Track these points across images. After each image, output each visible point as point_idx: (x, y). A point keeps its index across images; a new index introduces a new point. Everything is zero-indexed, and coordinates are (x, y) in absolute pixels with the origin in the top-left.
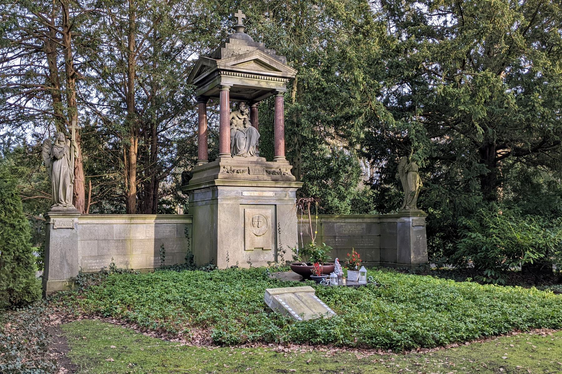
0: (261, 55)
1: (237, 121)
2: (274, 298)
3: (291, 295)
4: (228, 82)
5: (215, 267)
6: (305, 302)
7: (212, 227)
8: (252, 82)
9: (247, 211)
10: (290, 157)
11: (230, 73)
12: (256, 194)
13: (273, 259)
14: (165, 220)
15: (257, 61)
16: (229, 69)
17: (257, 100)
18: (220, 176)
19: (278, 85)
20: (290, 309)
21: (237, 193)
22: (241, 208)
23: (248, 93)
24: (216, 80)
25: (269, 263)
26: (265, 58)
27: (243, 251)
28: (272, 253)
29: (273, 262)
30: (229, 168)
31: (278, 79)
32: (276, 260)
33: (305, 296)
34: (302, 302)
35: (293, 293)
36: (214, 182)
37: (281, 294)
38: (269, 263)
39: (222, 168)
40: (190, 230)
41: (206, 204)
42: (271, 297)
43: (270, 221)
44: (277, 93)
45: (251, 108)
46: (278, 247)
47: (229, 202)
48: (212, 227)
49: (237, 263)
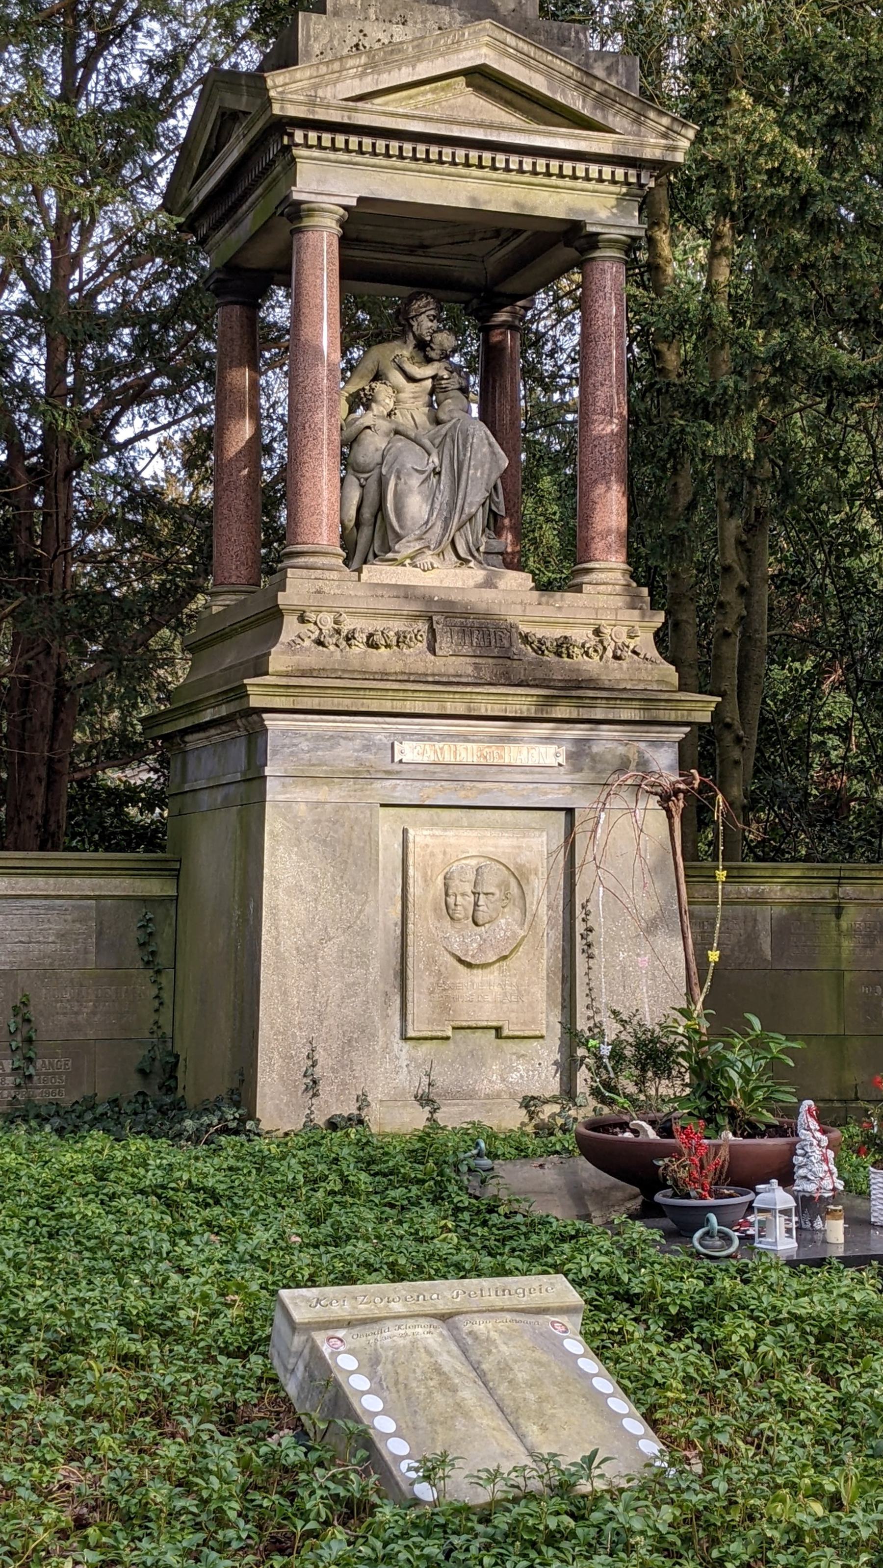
0: (502, 49)
1: (397, 390)
2: (315, 1350)
3: (429, 1335)
4: (328, 184)
5: (242, 1121)
6: (493, 1377)
7: (244, 918)
8: (461, 184)
9: (419, 837)
10: (652, 571)
11: (340, 140)
12: (468, 753)
13: (553, 1086)
14: (41, 881)
15: (482, 79)
16: (335, 116)
17: (512, 286)
18: (279, 660)
19: (597, 204)
20: (385, 1425)
21: (366, 748)
22: (387, 826)
23: (469, 257)
24: (276, 180)
25: (529, 1103)
26: (524, 60)
27: (397, 1043)
28: (549, 1052)
29: (554, 1100)
30: (327, 621)
31: (594, 169)
32: (569, 1093)
33: (508, 1336)
34: (482, 1376)
35: (444, 1317)
36: (241, 693)
37: (364, 1322)
38: (529, 1103)
39: (290, 624)
40: (168, 931)
41: (227, 804)
42: (298, 1341)
43: (544, 897)
44: (593, 241)
45: (485, 330)
46: (582, 1025)
47: (322, 793)
48: (244, 918)
49: (363, 1102)
